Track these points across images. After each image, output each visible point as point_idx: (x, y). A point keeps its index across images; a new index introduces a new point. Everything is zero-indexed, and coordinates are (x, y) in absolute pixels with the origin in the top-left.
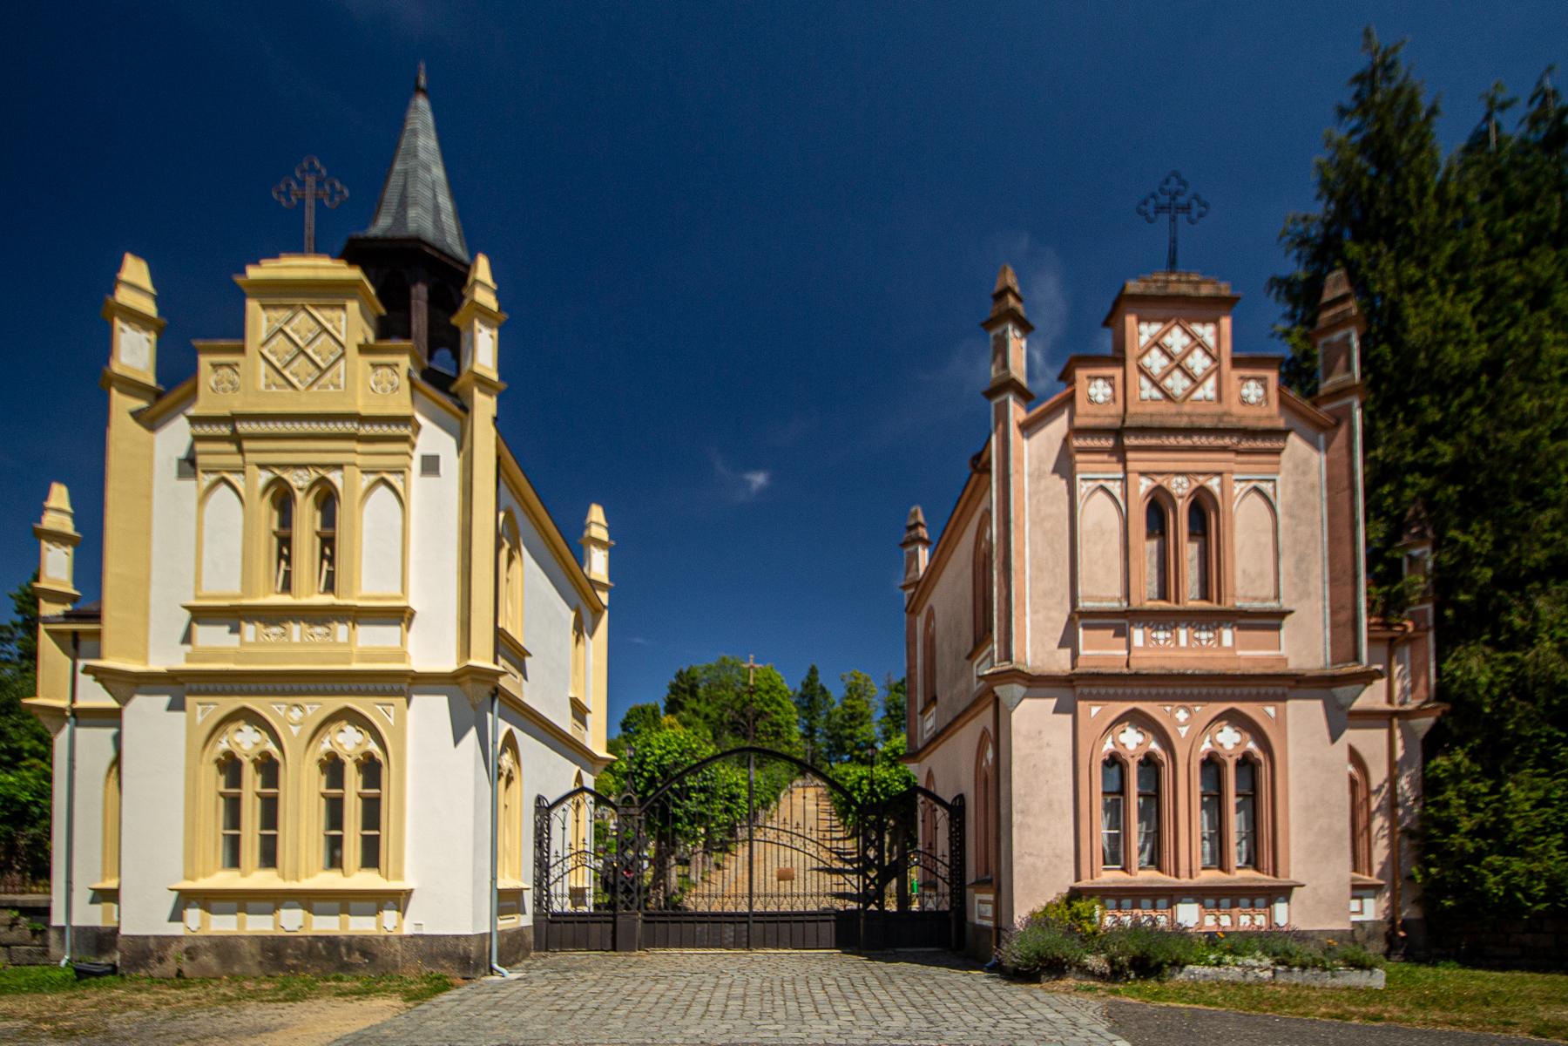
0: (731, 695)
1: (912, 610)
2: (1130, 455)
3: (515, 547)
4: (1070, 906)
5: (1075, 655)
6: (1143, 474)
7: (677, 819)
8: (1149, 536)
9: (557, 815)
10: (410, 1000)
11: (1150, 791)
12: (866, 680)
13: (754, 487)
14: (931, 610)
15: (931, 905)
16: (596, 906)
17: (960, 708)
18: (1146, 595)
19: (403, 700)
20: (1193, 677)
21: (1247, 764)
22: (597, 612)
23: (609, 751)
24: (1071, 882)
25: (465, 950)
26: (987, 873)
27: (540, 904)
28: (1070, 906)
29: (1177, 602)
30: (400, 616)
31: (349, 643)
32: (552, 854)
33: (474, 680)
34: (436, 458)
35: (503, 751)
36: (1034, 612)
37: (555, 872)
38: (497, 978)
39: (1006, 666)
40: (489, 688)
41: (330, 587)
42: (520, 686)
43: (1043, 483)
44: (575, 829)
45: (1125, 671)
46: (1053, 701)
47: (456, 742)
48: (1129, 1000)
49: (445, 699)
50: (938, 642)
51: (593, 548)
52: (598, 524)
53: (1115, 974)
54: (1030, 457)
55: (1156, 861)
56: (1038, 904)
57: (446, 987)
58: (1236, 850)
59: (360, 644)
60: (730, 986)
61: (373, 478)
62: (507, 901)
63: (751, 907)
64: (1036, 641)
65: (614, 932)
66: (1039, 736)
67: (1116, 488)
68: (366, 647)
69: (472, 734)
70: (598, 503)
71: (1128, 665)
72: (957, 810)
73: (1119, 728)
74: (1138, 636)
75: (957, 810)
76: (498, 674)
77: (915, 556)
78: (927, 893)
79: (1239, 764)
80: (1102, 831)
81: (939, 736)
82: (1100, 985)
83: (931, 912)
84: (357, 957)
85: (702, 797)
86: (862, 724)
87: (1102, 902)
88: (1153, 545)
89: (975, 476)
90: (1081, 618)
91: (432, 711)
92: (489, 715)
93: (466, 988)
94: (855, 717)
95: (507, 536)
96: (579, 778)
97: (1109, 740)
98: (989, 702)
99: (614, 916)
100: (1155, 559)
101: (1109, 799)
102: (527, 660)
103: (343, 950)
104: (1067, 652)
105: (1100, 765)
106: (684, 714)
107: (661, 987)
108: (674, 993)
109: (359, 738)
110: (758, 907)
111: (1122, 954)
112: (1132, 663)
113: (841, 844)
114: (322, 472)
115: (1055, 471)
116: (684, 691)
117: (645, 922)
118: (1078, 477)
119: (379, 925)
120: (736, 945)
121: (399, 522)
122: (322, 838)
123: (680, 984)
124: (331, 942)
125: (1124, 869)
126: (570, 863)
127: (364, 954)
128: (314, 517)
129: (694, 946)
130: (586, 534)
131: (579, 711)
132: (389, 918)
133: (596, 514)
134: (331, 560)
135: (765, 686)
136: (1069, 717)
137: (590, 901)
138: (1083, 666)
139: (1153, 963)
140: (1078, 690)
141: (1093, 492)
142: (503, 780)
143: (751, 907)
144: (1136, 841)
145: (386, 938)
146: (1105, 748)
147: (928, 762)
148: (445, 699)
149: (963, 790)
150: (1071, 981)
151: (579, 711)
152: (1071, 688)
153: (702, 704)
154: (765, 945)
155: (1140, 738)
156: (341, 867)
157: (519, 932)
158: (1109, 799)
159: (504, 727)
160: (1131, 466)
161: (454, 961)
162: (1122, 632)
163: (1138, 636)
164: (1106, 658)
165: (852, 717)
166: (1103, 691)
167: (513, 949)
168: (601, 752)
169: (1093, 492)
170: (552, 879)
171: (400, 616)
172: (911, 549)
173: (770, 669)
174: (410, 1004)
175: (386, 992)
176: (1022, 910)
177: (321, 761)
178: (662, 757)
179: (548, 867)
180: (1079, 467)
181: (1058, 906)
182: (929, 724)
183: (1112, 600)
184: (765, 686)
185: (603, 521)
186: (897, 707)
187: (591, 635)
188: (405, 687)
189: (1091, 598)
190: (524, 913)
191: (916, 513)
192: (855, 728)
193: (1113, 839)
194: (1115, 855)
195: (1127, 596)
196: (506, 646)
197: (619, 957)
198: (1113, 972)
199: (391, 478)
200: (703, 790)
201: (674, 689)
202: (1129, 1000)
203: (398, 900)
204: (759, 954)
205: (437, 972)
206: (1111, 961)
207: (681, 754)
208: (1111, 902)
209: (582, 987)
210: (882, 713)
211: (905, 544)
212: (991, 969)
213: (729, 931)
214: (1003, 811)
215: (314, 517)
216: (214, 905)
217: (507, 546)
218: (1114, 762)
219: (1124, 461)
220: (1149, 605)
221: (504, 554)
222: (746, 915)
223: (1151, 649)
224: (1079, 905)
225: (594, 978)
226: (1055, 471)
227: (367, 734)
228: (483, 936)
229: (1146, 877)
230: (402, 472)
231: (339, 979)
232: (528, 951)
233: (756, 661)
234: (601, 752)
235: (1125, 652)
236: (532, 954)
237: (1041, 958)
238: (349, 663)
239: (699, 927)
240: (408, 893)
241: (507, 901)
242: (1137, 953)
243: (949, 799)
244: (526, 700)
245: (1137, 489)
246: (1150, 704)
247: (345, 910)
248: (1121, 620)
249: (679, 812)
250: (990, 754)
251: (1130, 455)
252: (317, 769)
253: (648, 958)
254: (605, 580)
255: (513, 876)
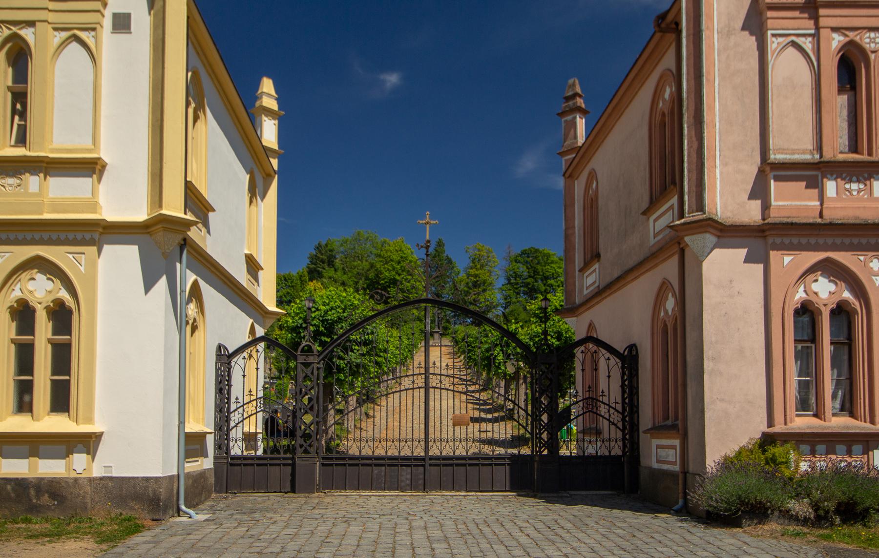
0: (366, 265)
1: (570, 175)
2: (822, 12)
3: (199, 108)
4: (764, 451)
5: (766, 207)
6: (835, 29)
7: (340, 370)
8: (841, 91)
9: (238, 363)
10: (102, 541)
11: (842, 339)
12: (489, 252)
13: (388, 85)
14: (593, 175)
15: (591, 450)
16: (265, 451)
17: (631, 263)
18: (837, 147)
19: (95, 248)
20: (792, 225)
21: (841, 311)
22: (268, 177)
23: (277, 306)
24: (764, 428)
25: (154, 491)
26: (666, 418)
27: (220, 447)
28: (764, 451)
29: (870, 154)
30: (91, 168)
31: (41, 192)
32: (233, 400)
33: (165, 229)
34: (128, 16)
35: (189, 301)
36: (724, 164)
37: (235, 418)
38: (184, 519)
39: (699, 216)
40: (178, 238)
41: (22, 140)
42: (204, 239)
43: (733, 39)
44: (251, 376)
45: (819, 220)
46: (744, 252)
47: (147, 290)
48: (842, 545)
49: (135, 249)
50: (601, 202)
51: (264, 118)
52: (269, 95)
53: (820, 519)
54: (719, 14)
55: (848, 407)
56: (731, 449)
57: (137, 529)
58: (830, 404)
59: (51, 195)
60: (425, 527)
61: (65, 35)
62: (192, 444)
63: (426, 450)
64: (727, 192)
65: (293, 474)
66: (729, 284)
67: (807, 44)
68: (57, 199)
69: (163, 282)
70: (269, 77)
71: (821, 215)
72: (629, 360)
73: (811, 277)
74: (831, 187)
75: (629, 360)
76: (188, 224)
77: (574, 124)
78: (587, 438)
79: (833, 312)
80: (793, 379)
81: (600, 293)
82: (805, 530)
83: (591, 457)
84: (45, 499)
85: (364, 350)
86: (484, 290)
87: (797, 449)
88: (844, 99)
89: (658, 35)
90: (771, 170)
91: (121, 262)
92: (178, 265)
93: (157, 530)
94: (477, 284)
95: (195, 94)
96: (252, 331)
97: (802, 289)
98: (678, 251)
99: (293, 459)
100: (845, 113)
101: (799, 347)
102: (211, 214)
103: (32, 492)
104: (757, 204)
105: (792, 312)
106: (324, 280)
107: (355, 529)
108: (372, 536)
109: (50, 285)
110: (434, 451)
111: (828, 499)
112: (826, 213)
113: (477, 395)
114: (14, 29)
115: (744, 28)
116: (323, 262)
117: (323, 465)
118: (769, 32)
119: (68, 467)
120: (413, 487)
121: (91, 77)
122: (12, 383)
123: (374, 526)
124: (21, 484)
125: (816, 415)
126: (250, 409)
127: (54, 495)
128: (6, 72)
129: (371, 489)
130: (258, 104)
131: (253, 266)
132: (79, 461)
133: (267, 86)
134: (23, 115)
135: (396, 257)
136: (760, 267)
137: (261, 445)
138: (775, 216)
139: (860, 508)
140: (770, 240)
141: (784, 47)
142: (189, 328)
143: (426, 450)
144: (829, 387)
145: (76, 480)
146: (797, 297)
147: (587, 317)
148: (135, 249)
149: (635, 340)
150: (773, 526)
151: (253, 266)
152: (763, 238)
153: (339, 273)
154: (441, 487)
155: (832, 287)
156: (30, 410)
157: (202, 475)
158: (799, 347)
159: (191, 277)
160: (823, 22)
161: (142, 502)
162: (814, 184)
163: (831, 187)
164: (798, 208)
165: (475, 285)
166: (795, 241)
167: (197, 490)
168: (272, 307)
169: (784, 47)
170: (232, 424)
171: (91, 168)
172: (569, 118)
173: (403, 243)
174: (104, 546)
175: (77, 534)
176: (713, 458)
177: (11, 307)
178: (326, 312)
179: (229, 412)
180: (770, 23)
181: (751, 451)
182: (591, 280)
183: (804, 152)
184: (396, 257)
185: (273, 92)
186: (516, 276)
187: (263, 198)
188: (96, 236)
189: (782, 151)
190: (207, 456)
191: (574, 85)
192: (479, 294)
193: (803, 387)
194: (806, 402)
195: (820, 148)
196: (195, 200)
197: (298, 500)
198: (818, 518)
199: (83, 35)
200: (366, 343)
201: (314, 259)
202: (842, 545)
203: (88, 443)
204: (437, 496)
205: (127, 513)
206: (816, 507)
207: (344, 310)
208: (805, 448)
209: (273, 528)
210: (503, 281)
211: (562, 114)
212: (678, 513)
213: (405, 474)
214: (690, 358)
215: (6, 72)
216: (42, 448)
217: (193, 105)
218: (806, 312)
219: (816, 18)
220: (841, 157)
221: (191, 111)
222: (423, 459)
223: (840, 199)
224: (777, 450)
225: (282, 518)
226: (744, 28)
227: (58, 282)
228: (171, 478)
229: (839, 423)
230: (94, 29)
231: (28, 521)
232: (210, 493)
233: (431, 219)
234: (272, 307)
235: (818, 203)
236: (214, 495)
237: (742, 503)
238: (42, 214)
239: (376, 470)
240: (98, 436)
241: (192, 444)
242: (844, 498)
243: (620, 347)
244: (209, 251)
245: (830, 44)
246: (849, 254)
247: (34, 453)
248: (813, 172)
249: (342, 363)
250: (670, 304)
251: (822, 12)
252: (7, 316)
253: (328, 500)
254: (275, 147)
255: (197, 421)
